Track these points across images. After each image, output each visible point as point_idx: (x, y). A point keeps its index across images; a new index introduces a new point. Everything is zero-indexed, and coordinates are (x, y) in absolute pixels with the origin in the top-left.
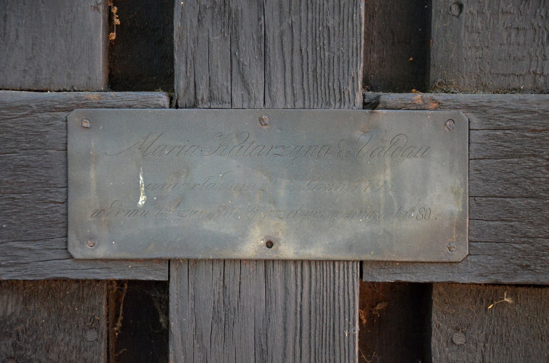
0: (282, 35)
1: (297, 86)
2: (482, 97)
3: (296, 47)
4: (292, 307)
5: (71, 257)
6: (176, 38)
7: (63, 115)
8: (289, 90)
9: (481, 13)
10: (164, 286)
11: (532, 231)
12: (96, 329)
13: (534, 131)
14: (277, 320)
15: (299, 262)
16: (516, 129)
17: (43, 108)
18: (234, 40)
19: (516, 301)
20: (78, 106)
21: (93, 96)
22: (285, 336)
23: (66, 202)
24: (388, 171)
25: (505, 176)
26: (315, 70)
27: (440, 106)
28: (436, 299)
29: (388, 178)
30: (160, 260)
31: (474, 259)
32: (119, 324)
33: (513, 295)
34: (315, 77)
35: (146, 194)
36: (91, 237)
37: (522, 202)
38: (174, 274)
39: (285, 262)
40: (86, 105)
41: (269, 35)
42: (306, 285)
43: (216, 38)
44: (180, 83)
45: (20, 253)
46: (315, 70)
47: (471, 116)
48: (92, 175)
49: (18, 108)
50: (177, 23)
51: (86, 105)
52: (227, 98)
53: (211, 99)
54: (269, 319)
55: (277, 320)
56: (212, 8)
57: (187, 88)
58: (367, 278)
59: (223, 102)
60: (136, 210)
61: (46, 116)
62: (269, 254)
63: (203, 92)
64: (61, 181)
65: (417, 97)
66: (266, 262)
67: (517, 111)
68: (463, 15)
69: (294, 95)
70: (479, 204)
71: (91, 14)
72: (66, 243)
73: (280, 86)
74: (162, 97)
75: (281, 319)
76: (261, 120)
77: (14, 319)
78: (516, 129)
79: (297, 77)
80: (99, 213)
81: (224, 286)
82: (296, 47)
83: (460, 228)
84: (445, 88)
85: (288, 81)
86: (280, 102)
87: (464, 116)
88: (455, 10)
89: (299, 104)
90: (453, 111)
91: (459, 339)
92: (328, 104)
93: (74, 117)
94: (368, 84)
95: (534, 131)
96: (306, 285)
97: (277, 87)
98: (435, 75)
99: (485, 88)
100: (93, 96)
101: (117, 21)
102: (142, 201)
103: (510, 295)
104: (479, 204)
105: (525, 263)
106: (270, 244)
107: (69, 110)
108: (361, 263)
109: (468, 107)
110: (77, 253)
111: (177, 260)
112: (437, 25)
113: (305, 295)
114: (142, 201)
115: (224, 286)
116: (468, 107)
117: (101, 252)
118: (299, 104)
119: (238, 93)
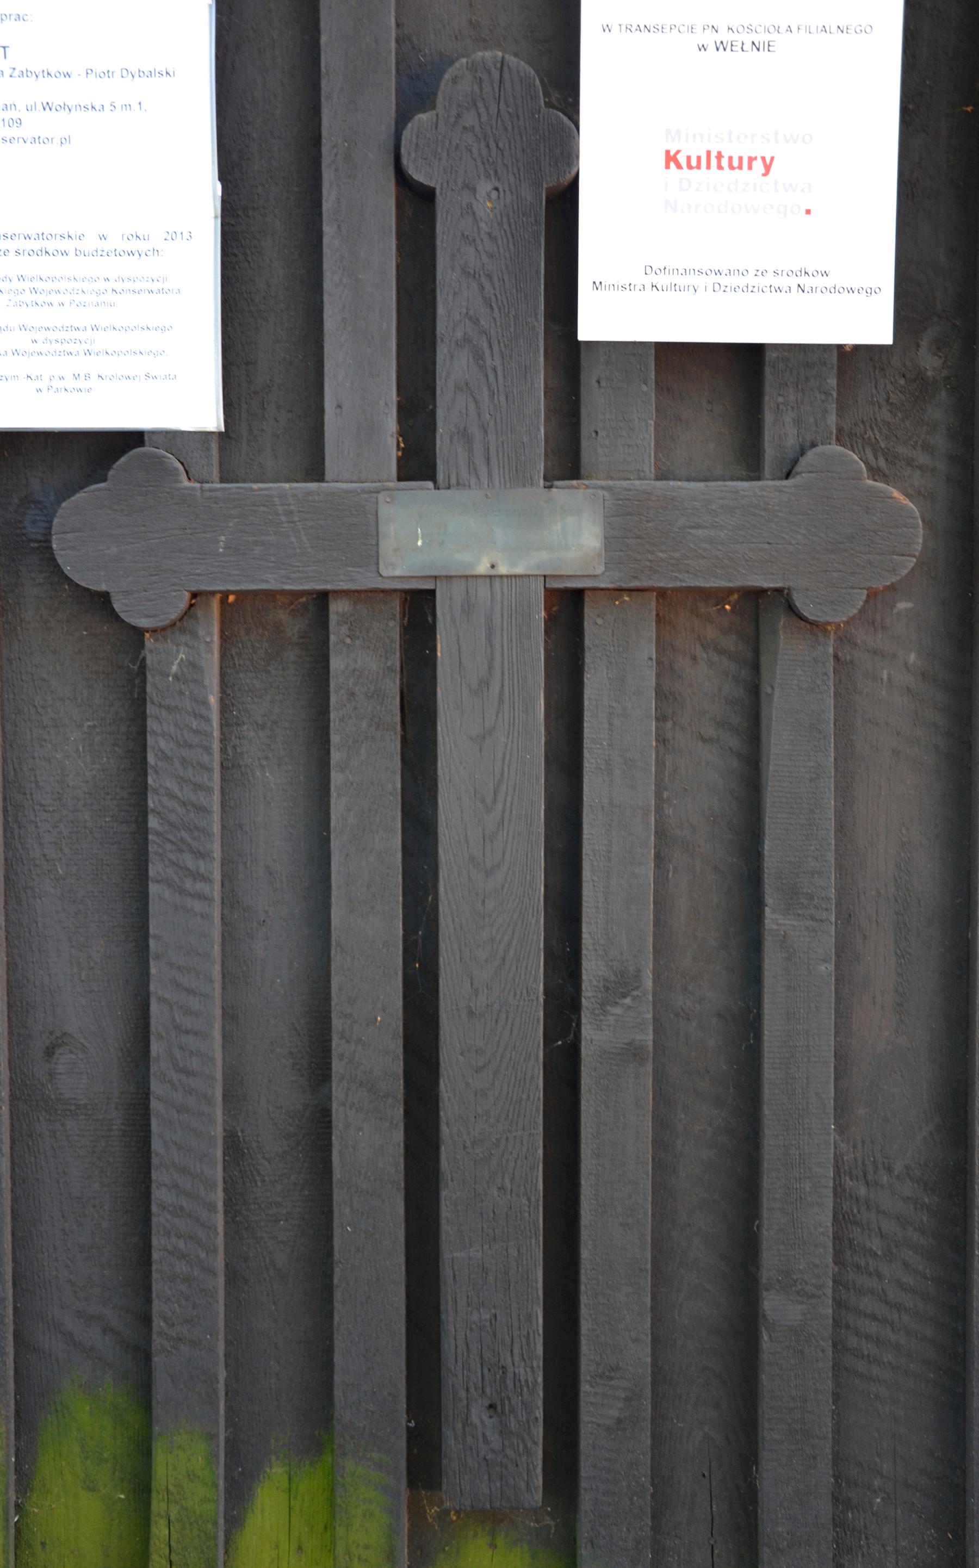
0: (497, 447)
1: (507, 476)
2: (610, 483)
3: (506, 454)
4: (506, 603)
5: (381, 576)
6: (438, 450)
7: (375, 495)
8: (502, 479)
9: (608, 436)
10: (432, 593)
11: (639, 557)
12: (395, 620)
13: (639, 501)
14: (497, 610)
15: (509, 577)
16: (629, 500)
17: (364, 492)
18: (470, 451)
19: (631, 600)
20: (383, 490)
21: (391, 484)
22: (502, 619)
23: (377, 544)
24: (559, 524)
25: (624, 526)
26: (516, 467)
27: (587, 487)
28: (587, 599)
29: (559, 528)
30: (430, 577)
31: (607, 574)
32: (406, 619)
33: (629, 596)
34: (516, 470)
35: (422, 539)
36: (392, 564)
37: (633, 541)
38: (438, 585)
39: (501, 577)
40: (388, 489)
41: (490, 448)
42: (514, 590)
43: (460, 450)
44: (440, 476)
45: (353, 574)
46: (516, 467)
47: (605, 493)
48: (392, 528)
49: (350, 492)
50: (438, 442)
51: (388, 489)
52: (467, 483)
53: (458, 484)
54: (507, 398)
55: (497, 610)
56: (458, 433)
57: (444, 479)
58: (548, 586)
59: (465, 485)
60: (417, 548)
61: (366, 496)
62: (493, 572)
63: (453, 481)
64: (375, 533)
65: (575, 482)
66: (491, 577)
67: (630, 490)
68: (599, 438)
69: (505, 481)
70: (610, 542)
71: (389, 439)
72: (378, 568)
73: (497, 476)
74: (430, 484)
75: (499, 609)
76: (487, 495)
77: (348, 614)
78: (629, 500)
79: (507, 471)
80: (396, 550)
81: (467, 592)
82: (506, 454)
83: (599, 556)
84: (587, 478)
85: (501, 473)
86: (497, 483)
87: (600, 492)
88: (594, 435)
89: (508, 486)
90: (595, 490)
91: (600, 621)
92: (524, 486)
93: (381, 497)
94: (545, 479)
95: (639, 501)
96: (514, 590)
97: (495, 471)
98: (583, 471)
99: (612, 478)
100: (391, 484)
101: (402, 445)
102: (420, 543)
103: (628, 596)
104: (610, 542)
105: (636, 575)
106: (493, 567)
107: (378, 492)
108: (545, 576)
109: (602, 488)
110: (384, 574)
111: (440, 577)
112: (584, 443)
113: (513, 595)
114: (420, 543)
115: (467, 592)
116: (602, 488)
117: (398, 573)
118: (508, 486)
119: (473, 481)
